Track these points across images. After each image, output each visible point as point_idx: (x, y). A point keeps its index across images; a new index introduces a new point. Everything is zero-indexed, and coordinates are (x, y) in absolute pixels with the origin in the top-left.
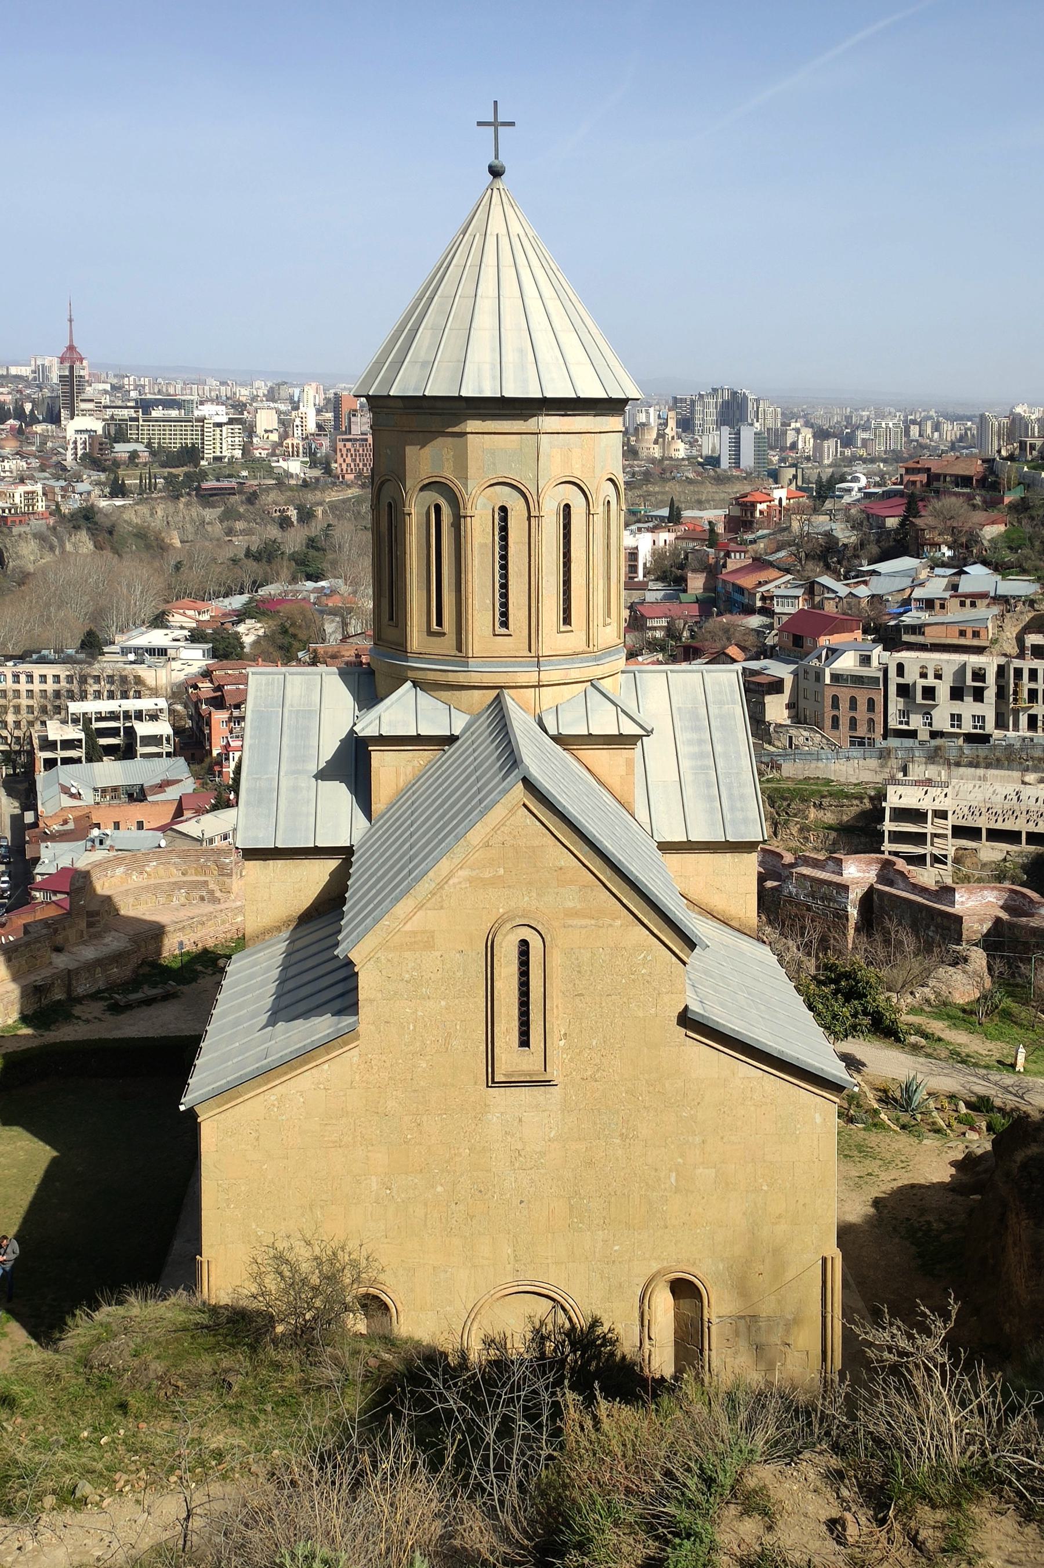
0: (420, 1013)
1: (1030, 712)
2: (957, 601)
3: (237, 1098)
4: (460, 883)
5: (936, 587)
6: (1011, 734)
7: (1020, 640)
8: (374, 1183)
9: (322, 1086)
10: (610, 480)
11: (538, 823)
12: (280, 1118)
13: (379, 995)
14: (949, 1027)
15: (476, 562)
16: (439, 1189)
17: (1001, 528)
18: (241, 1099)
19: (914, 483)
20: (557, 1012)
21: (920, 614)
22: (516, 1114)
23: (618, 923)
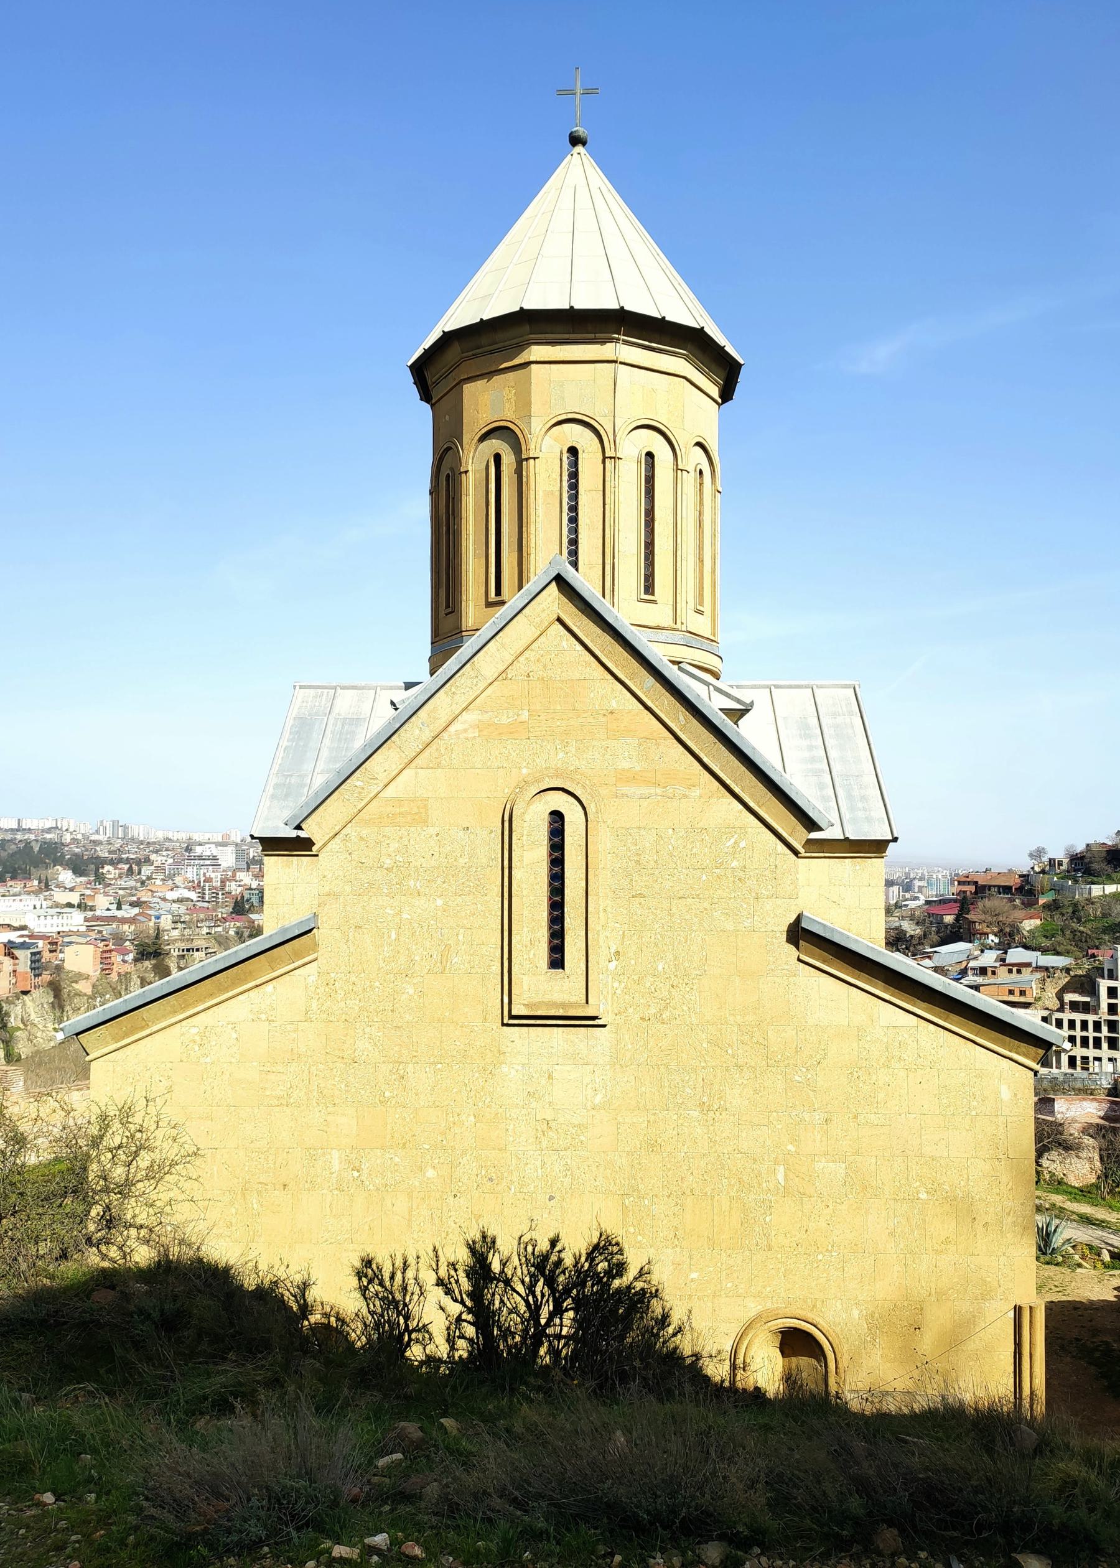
0: (405, 916)
1: (1070, 1054)
2: (1006, 968)
3: (143, 1028)
4: (465, 731)
5: (989, 958)
6: (1054, 1070)
7: (1060, 996)
8: (336, 1160)
9: (263, 1017)
10: (699, 444)
11: (579, 647)
12: (202, 1060)
13: (348, 888)
14: (1069, 1200)
15: (540, 512)
16: (431, 1173)
17: (1038, 922)
18: (148, 1032)
19: (965, 892)
20: (604, 916)
21: (976, 978)
22: (545, 1068)
23: (696, 792)
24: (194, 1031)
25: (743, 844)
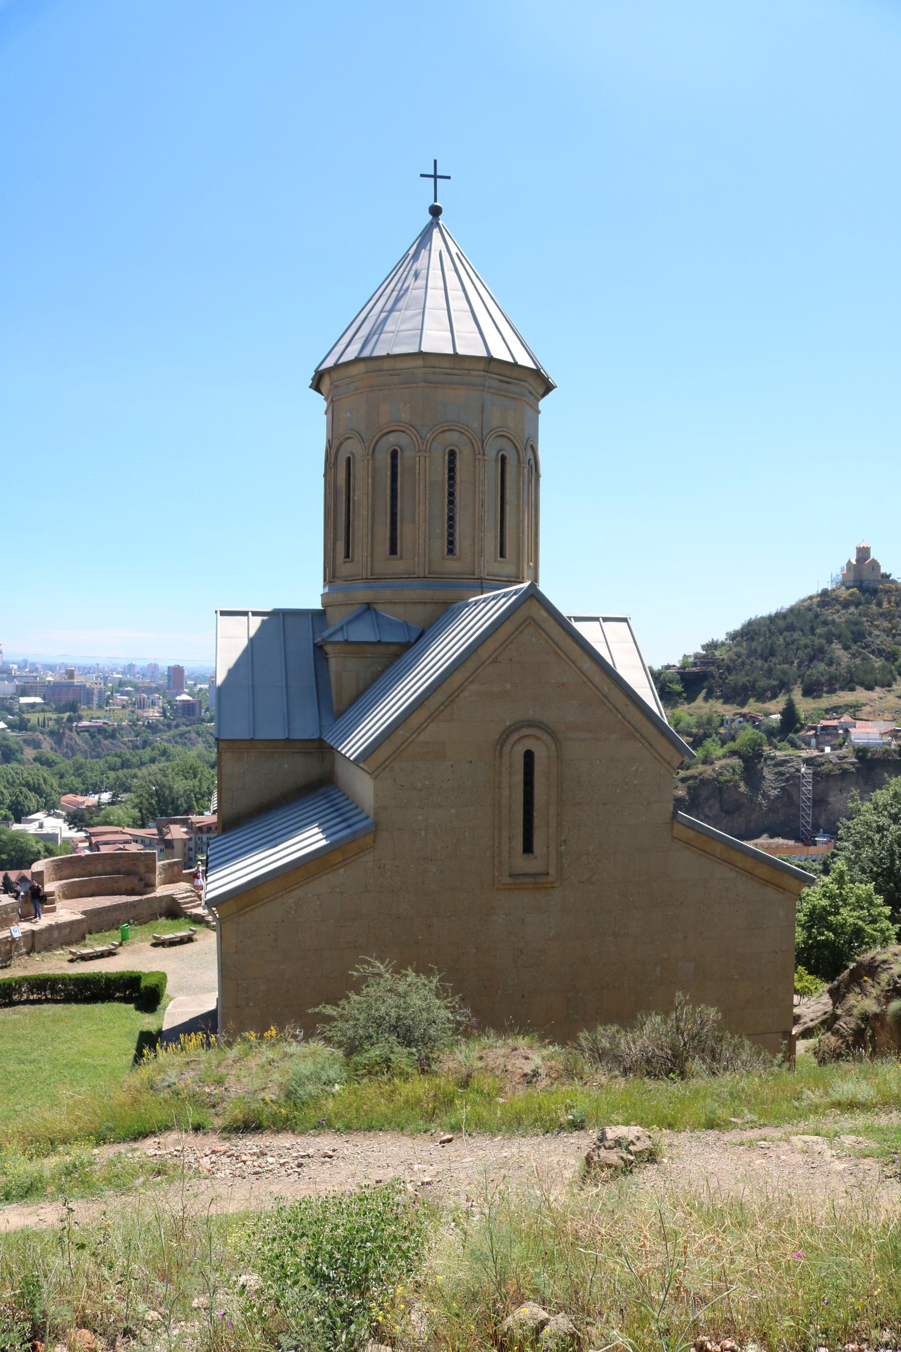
9: (338, 890)
24: (291, 901)
25: (641, 769)
